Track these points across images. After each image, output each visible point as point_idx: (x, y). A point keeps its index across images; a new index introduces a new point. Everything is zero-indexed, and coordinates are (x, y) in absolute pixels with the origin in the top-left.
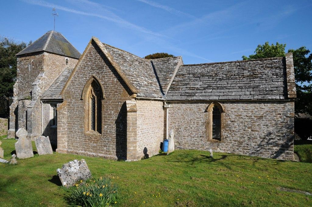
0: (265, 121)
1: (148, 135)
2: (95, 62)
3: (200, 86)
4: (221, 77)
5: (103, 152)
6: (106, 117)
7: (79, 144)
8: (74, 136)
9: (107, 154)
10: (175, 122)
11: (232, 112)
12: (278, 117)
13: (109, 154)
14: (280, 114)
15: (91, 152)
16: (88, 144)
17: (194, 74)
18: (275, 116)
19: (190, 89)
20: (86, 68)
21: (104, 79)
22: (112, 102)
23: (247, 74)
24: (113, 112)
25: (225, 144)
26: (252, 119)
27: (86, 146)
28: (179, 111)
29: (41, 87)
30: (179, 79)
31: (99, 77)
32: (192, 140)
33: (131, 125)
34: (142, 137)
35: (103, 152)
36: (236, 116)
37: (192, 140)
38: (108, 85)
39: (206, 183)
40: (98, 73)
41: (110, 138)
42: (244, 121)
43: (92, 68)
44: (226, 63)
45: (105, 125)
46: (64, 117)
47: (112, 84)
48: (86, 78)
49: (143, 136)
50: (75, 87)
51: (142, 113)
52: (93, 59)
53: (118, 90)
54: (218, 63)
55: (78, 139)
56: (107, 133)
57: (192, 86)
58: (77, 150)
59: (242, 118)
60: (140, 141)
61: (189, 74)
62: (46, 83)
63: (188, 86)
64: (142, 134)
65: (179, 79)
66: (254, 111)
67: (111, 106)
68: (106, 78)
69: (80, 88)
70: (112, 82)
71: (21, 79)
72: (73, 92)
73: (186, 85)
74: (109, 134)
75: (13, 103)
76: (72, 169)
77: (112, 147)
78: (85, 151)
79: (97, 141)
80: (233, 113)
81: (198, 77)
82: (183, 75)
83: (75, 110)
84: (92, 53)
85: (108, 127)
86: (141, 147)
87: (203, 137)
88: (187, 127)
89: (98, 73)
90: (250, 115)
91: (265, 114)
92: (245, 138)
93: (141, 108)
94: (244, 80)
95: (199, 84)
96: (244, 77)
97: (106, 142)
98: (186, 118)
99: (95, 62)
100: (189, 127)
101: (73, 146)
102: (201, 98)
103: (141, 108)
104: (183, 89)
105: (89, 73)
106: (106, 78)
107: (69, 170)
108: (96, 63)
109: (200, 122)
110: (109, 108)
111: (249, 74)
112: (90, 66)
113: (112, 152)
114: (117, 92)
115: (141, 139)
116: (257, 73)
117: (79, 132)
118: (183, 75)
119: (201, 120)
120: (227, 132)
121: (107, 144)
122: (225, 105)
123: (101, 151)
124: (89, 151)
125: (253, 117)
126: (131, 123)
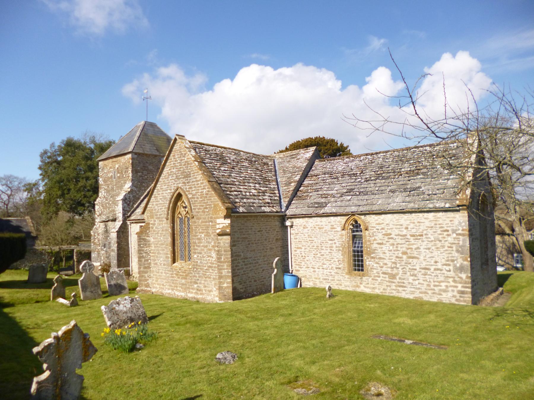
0: (427, 242)
1: (255, 266)
2: (180, 168)
3: (336, 192)
4: (367, 176)
5: (194, 291)
6: (196, 243)
7: (165, 281)
8: (159, 270)
9: (197, 293)
10: (300, 246)
11: (378, 229)
12: (444, 236)
13: (201, 294)
14: (448, 231)
15: (180, 291)
16: (176, 280)
17: (331, 174)
18: (440, 234)
19: (322, 196)
20: (170, 176)
21: (192, 191)
22: (202, 222)
23: (406, 169)
24: (203, 235)
25: (371, 279)
26: (407, 239)
27: (173, 283)
28: (306, 230)
29: (128, 203)
30: (310, 182)
31: (186, 188)
32: (325, 273)
33: (223, 252)
34: (244, 270)
35: (194, 291)
36: (384, 235)
37: (325, 273)
38: (196, 199)
39: (306, 331)
40: (184, 183)
41: (201, 272)
42: (395, 243)
43: (176, 176)
44: (380, 153)
45: (195, 253)
46: (146, 244)
47: (201, 198)
48: (171, 190)
49: (247, 268)
50: (158, 203)
51: (244, 236)
52: (178, 165)
53: (208, 205)
54: (367, 155)
55: (164, 274)
56: (197, 265)
57: (325, 192)
58: (163, 289)
59: (392, 238)
60: (242, 275)
61: (325, 174)
62: (135, 196)
63: (320, 193)
64: (246, 265)
65: (310, 182)
66: (409, 227)
67: (201, 227)
68: (193, 189)
69: (164, 204)
70: (201, 195)
71: (105, 193)
72: (155, 210)
73: (318, 191)
74: (200, 266)
75: (95, 226)
76: (121, 307)
77: (204, 284)
78: (173, 290)
79: (186, 275)
80: (379, 231)
81: (337, 178)
82: (316, 176)
83: (159, 235)
84: (176, 157)
85: (198, 256)
86: (243, 284)
87: (340, 268)
88: (317, 254)
89: (184, 183)
90: (404, 233)
91: (425, 232)
92: (398, 268)
93: (241, 229)
94: (400, 179)
95: (336, 189)
96: (401, 175)
97: (196, 277)
98: (315, 239)
99: (180, 168)
100: (319, 254)
101: (158, 284)
102: (334, 210)
103: (241, 229)
104: (312, 198)
105: (174, 184)
106: (193, 189)
107: (117, 308)
108: (182, 169)
109: (334, 245)
110: (199, 230)
111: (409, 169)
112: (175, 174)
113: (204, 291)
114: (206, 208)
115: (243, 273)
116: (422, 168)
117: (164, 265)
118: (316, 176)
119: (335, 243)
120: (372, 260)
121: (198, 280)
122: (345, 220)
123: (191, 290)
124: (177, 290)
125: (409, 237)
126: (223, 249)
